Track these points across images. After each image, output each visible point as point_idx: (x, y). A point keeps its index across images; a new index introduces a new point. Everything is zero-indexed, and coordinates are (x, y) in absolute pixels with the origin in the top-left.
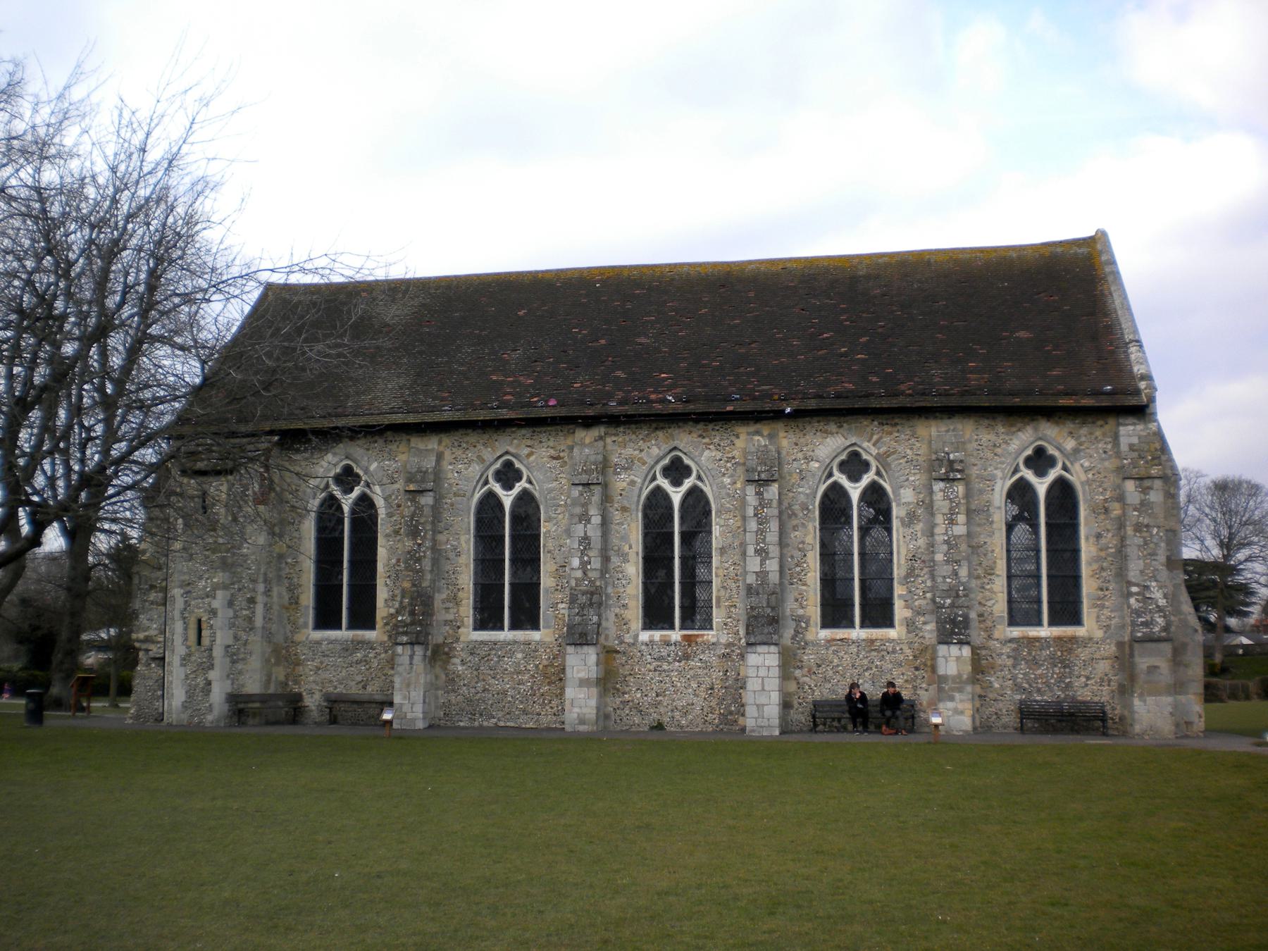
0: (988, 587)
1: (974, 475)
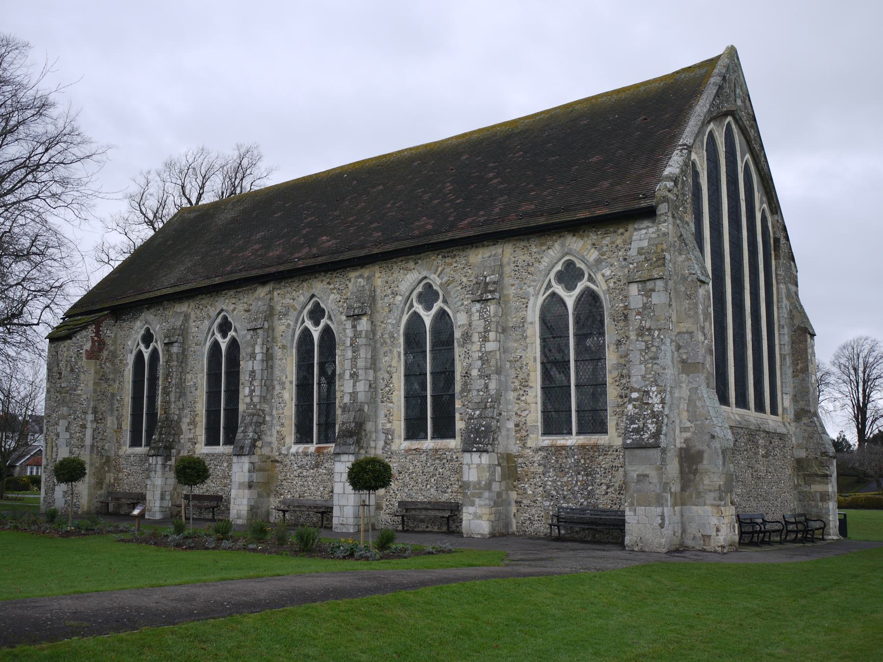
0: (523, 398)
1: (512, 295)
